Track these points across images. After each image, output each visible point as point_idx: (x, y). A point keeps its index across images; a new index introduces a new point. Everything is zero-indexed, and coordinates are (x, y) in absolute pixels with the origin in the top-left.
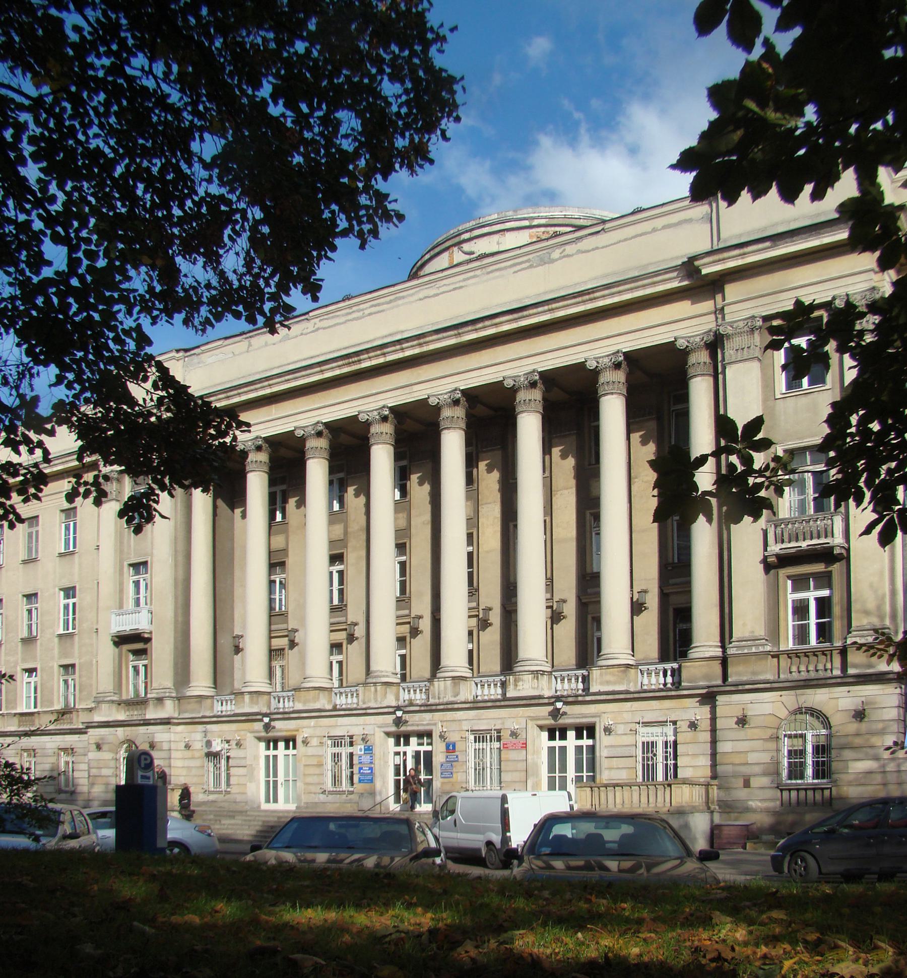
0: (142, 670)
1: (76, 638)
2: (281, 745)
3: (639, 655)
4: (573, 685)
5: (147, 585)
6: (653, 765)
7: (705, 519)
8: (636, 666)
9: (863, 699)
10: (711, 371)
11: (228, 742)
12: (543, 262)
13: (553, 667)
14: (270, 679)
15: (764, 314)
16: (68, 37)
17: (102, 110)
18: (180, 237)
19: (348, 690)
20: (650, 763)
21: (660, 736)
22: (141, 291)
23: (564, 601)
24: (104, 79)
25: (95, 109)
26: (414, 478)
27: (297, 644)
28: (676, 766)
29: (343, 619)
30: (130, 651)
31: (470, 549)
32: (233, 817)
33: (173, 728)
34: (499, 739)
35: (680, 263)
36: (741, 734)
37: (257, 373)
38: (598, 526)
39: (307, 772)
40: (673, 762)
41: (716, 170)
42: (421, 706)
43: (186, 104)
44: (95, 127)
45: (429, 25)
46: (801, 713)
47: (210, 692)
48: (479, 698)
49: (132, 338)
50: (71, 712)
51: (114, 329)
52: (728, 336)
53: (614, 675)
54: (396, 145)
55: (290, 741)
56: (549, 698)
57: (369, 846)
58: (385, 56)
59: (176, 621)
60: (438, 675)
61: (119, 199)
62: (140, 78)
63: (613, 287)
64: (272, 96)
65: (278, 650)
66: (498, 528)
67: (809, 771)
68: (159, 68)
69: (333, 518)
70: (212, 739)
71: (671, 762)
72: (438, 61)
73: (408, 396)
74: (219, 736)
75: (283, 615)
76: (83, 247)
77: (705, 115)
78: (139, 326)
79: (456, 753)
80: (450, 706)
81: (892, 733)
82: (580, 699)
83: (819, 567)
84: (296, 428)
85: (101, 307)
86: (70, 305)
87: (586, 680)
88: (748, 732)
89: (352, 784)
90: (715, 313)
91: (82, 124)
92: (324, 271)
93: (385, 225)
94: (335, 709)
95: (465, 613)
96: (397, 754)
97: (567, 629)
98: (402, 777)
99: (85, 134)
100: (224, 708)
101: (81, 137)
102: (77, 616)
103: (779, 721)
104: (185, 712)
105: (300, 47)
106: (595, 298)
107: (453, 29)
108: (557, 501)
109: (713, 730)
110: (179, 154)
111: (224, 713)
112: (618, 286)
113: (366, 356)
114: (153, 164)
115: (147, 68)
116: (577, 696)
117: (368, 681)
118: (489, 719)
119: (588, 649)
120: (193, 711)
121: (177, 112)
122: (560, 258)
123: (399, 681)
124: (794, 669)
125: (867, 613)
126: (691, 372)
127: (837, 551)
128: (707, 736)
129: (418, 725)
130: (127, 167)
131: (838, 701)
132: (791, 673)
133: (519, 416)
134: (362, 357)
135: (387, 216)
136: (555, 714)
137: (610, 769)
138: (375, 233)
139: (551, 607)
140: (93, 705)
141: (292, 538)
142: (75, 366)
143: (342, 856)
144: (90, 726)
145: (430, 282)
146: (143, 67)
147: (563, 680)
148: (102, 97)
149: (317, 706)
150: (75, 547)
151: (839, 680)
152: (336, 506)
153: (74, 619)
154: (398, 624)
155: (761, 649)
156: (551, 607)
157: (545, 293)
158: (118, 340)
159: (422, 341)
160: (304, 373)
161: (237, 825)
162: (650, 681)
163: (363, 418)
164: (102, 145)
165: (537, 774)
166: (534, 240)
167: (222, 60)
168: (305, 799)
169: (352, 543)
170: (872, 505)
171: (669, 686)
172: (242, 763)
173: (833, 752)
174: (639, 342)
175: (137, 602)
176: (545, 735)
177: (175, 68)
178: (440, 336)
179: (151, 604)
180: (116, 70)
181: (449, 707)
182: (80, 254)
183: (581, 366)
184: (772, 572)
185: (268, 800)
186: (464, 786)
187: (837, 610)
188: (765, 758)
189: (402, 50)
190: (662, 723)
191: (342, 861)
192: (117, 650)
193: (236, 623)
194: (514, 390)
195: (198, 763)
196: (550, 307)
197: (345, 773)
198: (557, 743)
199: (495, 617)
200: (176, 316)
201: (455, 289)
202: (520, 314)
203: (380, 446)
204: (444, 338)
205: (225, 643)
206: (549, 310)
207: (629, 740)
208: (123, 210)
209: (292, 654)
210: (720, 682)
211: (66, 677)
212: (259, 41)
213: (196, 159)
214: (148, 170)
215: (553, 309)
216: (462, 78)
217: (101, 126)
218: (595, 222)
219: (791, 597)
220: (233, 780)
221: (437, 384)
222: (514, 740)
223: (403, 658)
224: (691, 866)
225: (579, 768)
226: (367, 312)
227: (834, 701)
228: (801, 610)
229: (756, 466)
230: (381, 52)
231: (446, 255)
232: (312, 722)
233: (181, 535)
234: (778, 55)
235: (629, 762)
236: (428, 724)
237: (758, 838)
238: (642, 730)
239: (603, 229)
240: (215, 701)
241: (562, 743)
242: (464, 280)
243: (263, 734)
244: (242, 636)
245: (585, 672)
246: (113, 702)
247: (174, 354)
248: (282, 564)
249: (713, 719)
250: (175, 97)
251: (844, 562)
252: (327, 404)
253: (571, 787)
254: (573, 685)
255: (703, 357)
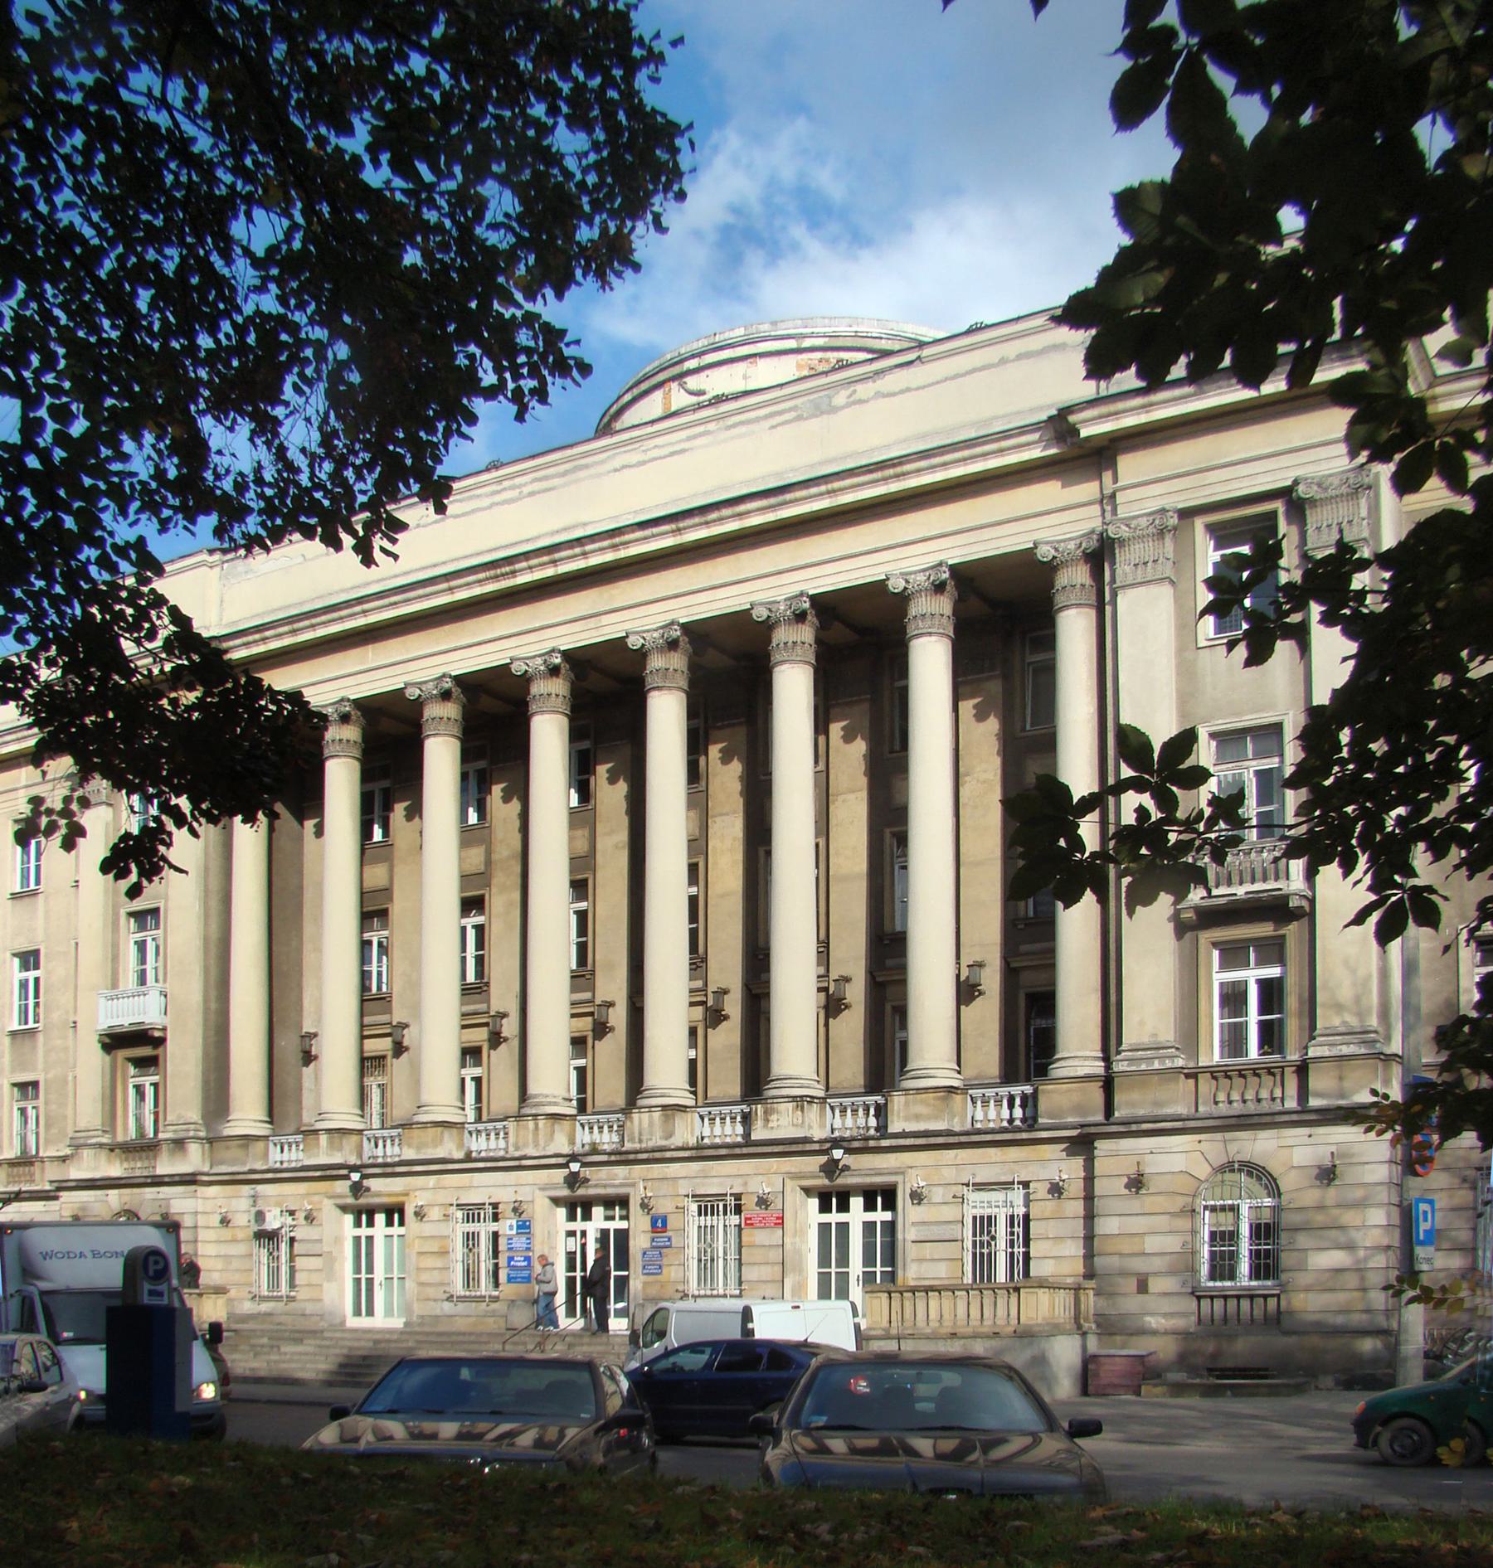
0: (150, 1092)
1: (41, 1037)
2: (380, 1218)
3: (969, 1071)
4: (861, 1121)
5: (157, 947)
6: (990, 1254)
7: (1094, 898)
8: (964, 1090)
9: (1333, 1148)
10: (1093, 600)
11: (292, 1213)
12: (819, 411)
13: (827, 1089)
14: (362, 1108)
15: (1180, 506)
16: (18, 31)
17: (78, 160)
18: (209, 384)
19: (490, 1126)
20: (985, 1251)
21: (1002, 1206)
22: (144, 476)
23: (847, 980)
24: (81, 109)
25: (66, 159)
26: (602, 770)
27: (407, 1049)
28: (1027, 1257)
29: (482, 1007)
30: (129, 1060)
31: (694, 890)
32: (299, 1341)
33: (202, 1190)
34: (738, 1210)
35: (1044, 417)
36: (1135, 1205)
37: (343, 591)
38: (905, 855)
39: (422, 1265)
40: (1022, 1250)
41: (1122, 325)
42: (610, 1154)
43: (223, 155)
44: (66, 190)
45: (635, 34)
46: (1232, 1171)
47: (262, 1130)
48: (706, 1141)
49: (128, 559)
50: (32, 1164)
51: (98, 543)
52: (1122, 542)
53: (928, 1105)
54: (578, 238)
55: (394, 1212)
56: (820, 1142)
57: (525, 1406)
58: (560, 84)
59: (206, 1010)
60: (640, 1103)
61: (106, 315)
62: (146, 109)
63: (934, 456)
64: (369, 148)
65: (375, 1058)
66: (739, 855)
67: (1244, 1267)
68: (177, 92)
69: (468, 836)
70: (265, 1209)
71: (1019, 1250)
72: (652, 96)
73: (593, 633)
74: (278, 1204)
75: (384, 1000)
76: (48, 400)
77: (1109, 240)
78: (141, 540)
79: (669, 1234)
80: (657, 1155)
81: (1379, 1205)
82: (872, 1143)
83: (1265, 929)
84: (407, 685)
85: (76, 505)
86: (24, 500)
87: (881, 1112)
88: (1147, 1202)
89: (497, 1284)
90: (1101, 502)
91: (45, 185)
92: (456, 458)
93: (558, 381)
94: (468, 1158)
95: (684, 998)
96: (571, 1234)
97: (852, 1026)
98: (578, 1274)
99: (50, 202)
100: (286, 1156)
101: (43, 208)
102: (41, 1000)
103: (1196, 1183)
104: (222, 1163)
105: (418, 64)
106: (904, 474)
107: (677, 43)
108: (838, 812)
109: (1089, 1197)
110: (209, 240)
111: (285, 1165)
112: (942, 454)
113: (524, 564)
114: (165, 257)
115: (157, 93)
116: (867, 1139)
117: (524, 1111)
118: (722, 1177)
119: (886, 1060)
120: (233, 1162)
121: (205, 167)
122: (848, 405)
123: (574, 1112)
124: (1221, 1097)
125: (1339, 1007)
126: (1060, 600)
127: (1294, 903)
128: (1078, 1207)
129: (605, 1186)
130: (121, 259)
131: (1292, 1151)
132: (1216, 1103)
133: (776, 670)
134: (518, 566)
135: (562, 367)
136: (831, 1169)
137: (920, 1260)
138: (541, 394)
139: (826, 989)
140: (68, 1151)
141: (399, 870)
142: (30, 604)
143: (482, 1426)
144: (63, 1186)
145: (632, 441)
146: (150, 89)
147: (843, 1111)
148: (79, 138)
149: (440, 1153)
150: (38, 882)
151: (1295, 1117)
152: (473, 817)
153: (37, 1005)
154: (573, 1016)
155: (1168, 1064)
156: (826, 989)
157: (821, 463)
158: (105, 563)
159: (617, 540)
160: (421, 592)
161: (306, 1354)
162: (986, 1114)
163: (518, 668)
164: (78, 221)
165: (800, 1269)
166: (806, 373)
167: (285, 81)
168: (419, 1309)
169: (498, 879)
170: (1369, 875)
171: (1018, 1123)
172: (316, 1249)
173: (1283, 1235)
174: (975, 548)
175: (142, 979)
176: (814, 1203)
177: (204, 92)
178: (648, 532)
179: (165, 981)
180: (106, 93)
181: (656, 1156)
182: (43, 413)
183: (879, 587)
184: (1188, 935)
185: (357, 1312)
186: (680, 1288)
187: (1292, 1001)
188: (1173, 1244)
189: (589, 75)
190: (1007, 1185)
191: (480, 1436)
192: (108, 1058)
193: (305, 1013)
194: (768, 626)
195: (239, 1249)
196: (830, 486)
197: (485, 1266)
198: (834, 1217)
199: (734, 1006)
200: (202, 519)
201: (672, 454)
202: (780, 499)
203: (547, 716)
204: (654, 536)
205: (288, 1045)
206: (828, 492)
207: (950, 1213)
208: (114, 335)
209: (398, 1066)
210: (1100, 1118)
211: (22, 1104)
212: (349, 49)
213: (239, 251)
214: (156, 266)
215: (834, 491)
216: (690, 126)
217: (78, 189)
218: (906, 345)
219: (1219, 978)
220: (300, 1278)
221: (640, 613)
222: (763, 1213)
223: (581, 1072)
224: (1052, 1446)
225: (869, 1260)
226: (526, 490)
227: (1285, 1151)
228: (1234, 999)
229: (1180, 814)
230: (554, 76)
231: (658, 395)
232: (432, 1180)
233: (215, 864)
234: (1241, 139)
235: (951, 1250)
236: (622, 1185)
237: (1159, 1376)
238: (973, 1197)
239: (919, 358)
240: (271, 1145)
241: (843, 1217)
242: (689, 439)
243: (350, 1201)
244: (315, 1035)
245: (879, 1099)
246: (101, 1146)
247: (205, 557)
248: (383, 914)
249: (1089, 1179)
250: (203, 144)
251: (1305, 921)
252: (459, 644)
253: (856, 1292)
254: (861, 1121)
255: (1077, 576)
